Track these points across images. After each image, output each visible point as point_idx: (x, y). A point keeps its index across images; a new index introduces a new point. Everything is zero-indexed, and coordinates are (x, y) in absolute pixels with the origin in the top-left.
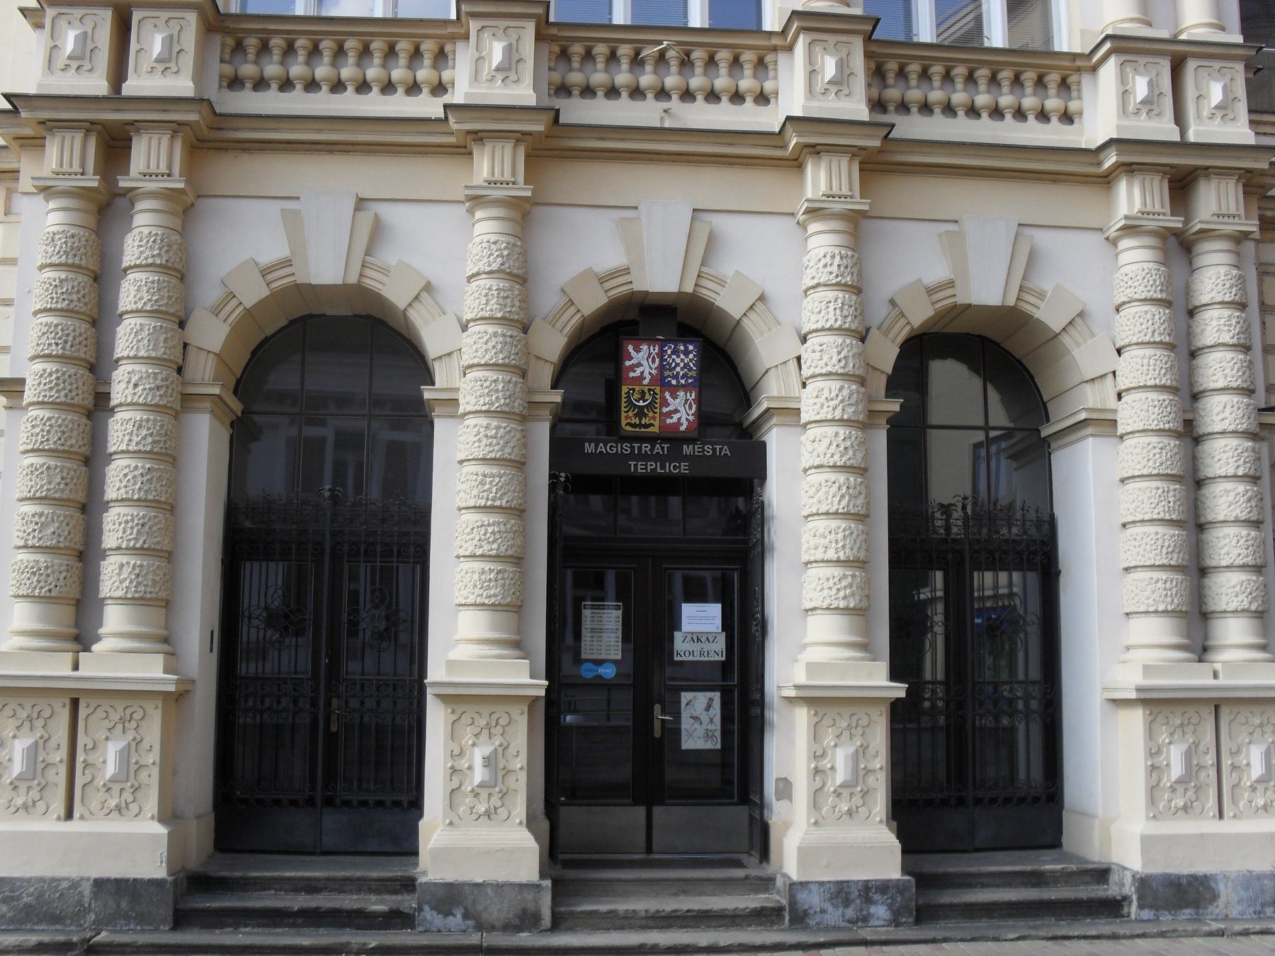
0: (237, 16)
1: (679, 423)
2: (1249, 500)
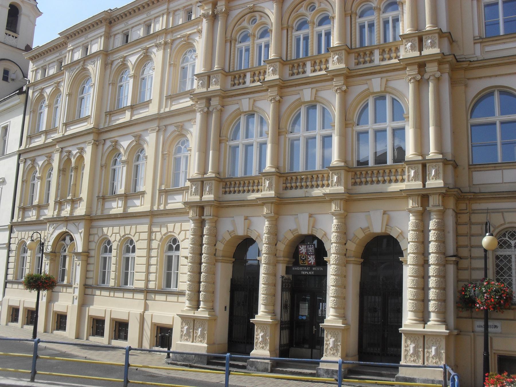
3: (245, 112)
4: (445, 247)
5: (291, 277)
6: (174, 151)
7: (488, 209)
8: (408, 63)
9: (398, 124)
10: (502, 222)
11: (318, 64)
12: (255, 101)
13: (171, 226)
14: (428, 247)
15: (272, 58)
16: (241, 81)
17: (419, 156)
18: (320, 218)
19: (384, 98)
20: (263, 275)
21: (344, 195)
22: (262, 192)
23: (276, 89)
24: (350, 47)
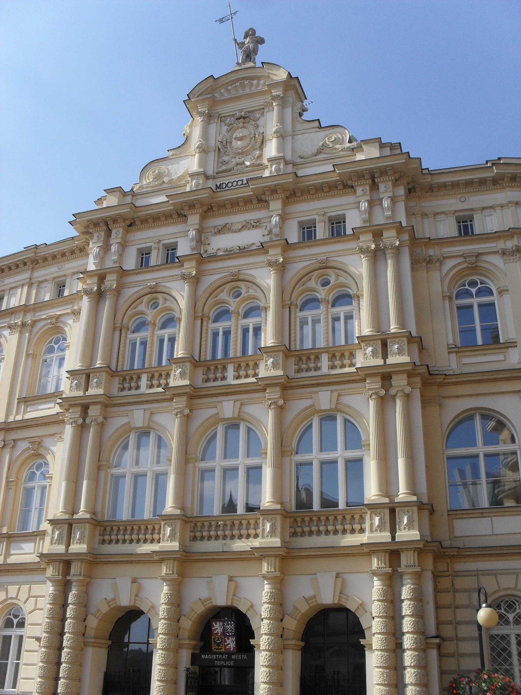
2: (416, 676)
3: (138, 428)
4: (424, 625)
5: (196, 669)
7: (477, 571)
8: (366, 374)
9: (253, 461)
10: (496, 588)
12: (152, 413)
13: (13, 590)
14: (401, 624)
15: (179, 356)
18: (244, 582)
19: (333, 418)
21: (281, 549)
23: (185, 398)
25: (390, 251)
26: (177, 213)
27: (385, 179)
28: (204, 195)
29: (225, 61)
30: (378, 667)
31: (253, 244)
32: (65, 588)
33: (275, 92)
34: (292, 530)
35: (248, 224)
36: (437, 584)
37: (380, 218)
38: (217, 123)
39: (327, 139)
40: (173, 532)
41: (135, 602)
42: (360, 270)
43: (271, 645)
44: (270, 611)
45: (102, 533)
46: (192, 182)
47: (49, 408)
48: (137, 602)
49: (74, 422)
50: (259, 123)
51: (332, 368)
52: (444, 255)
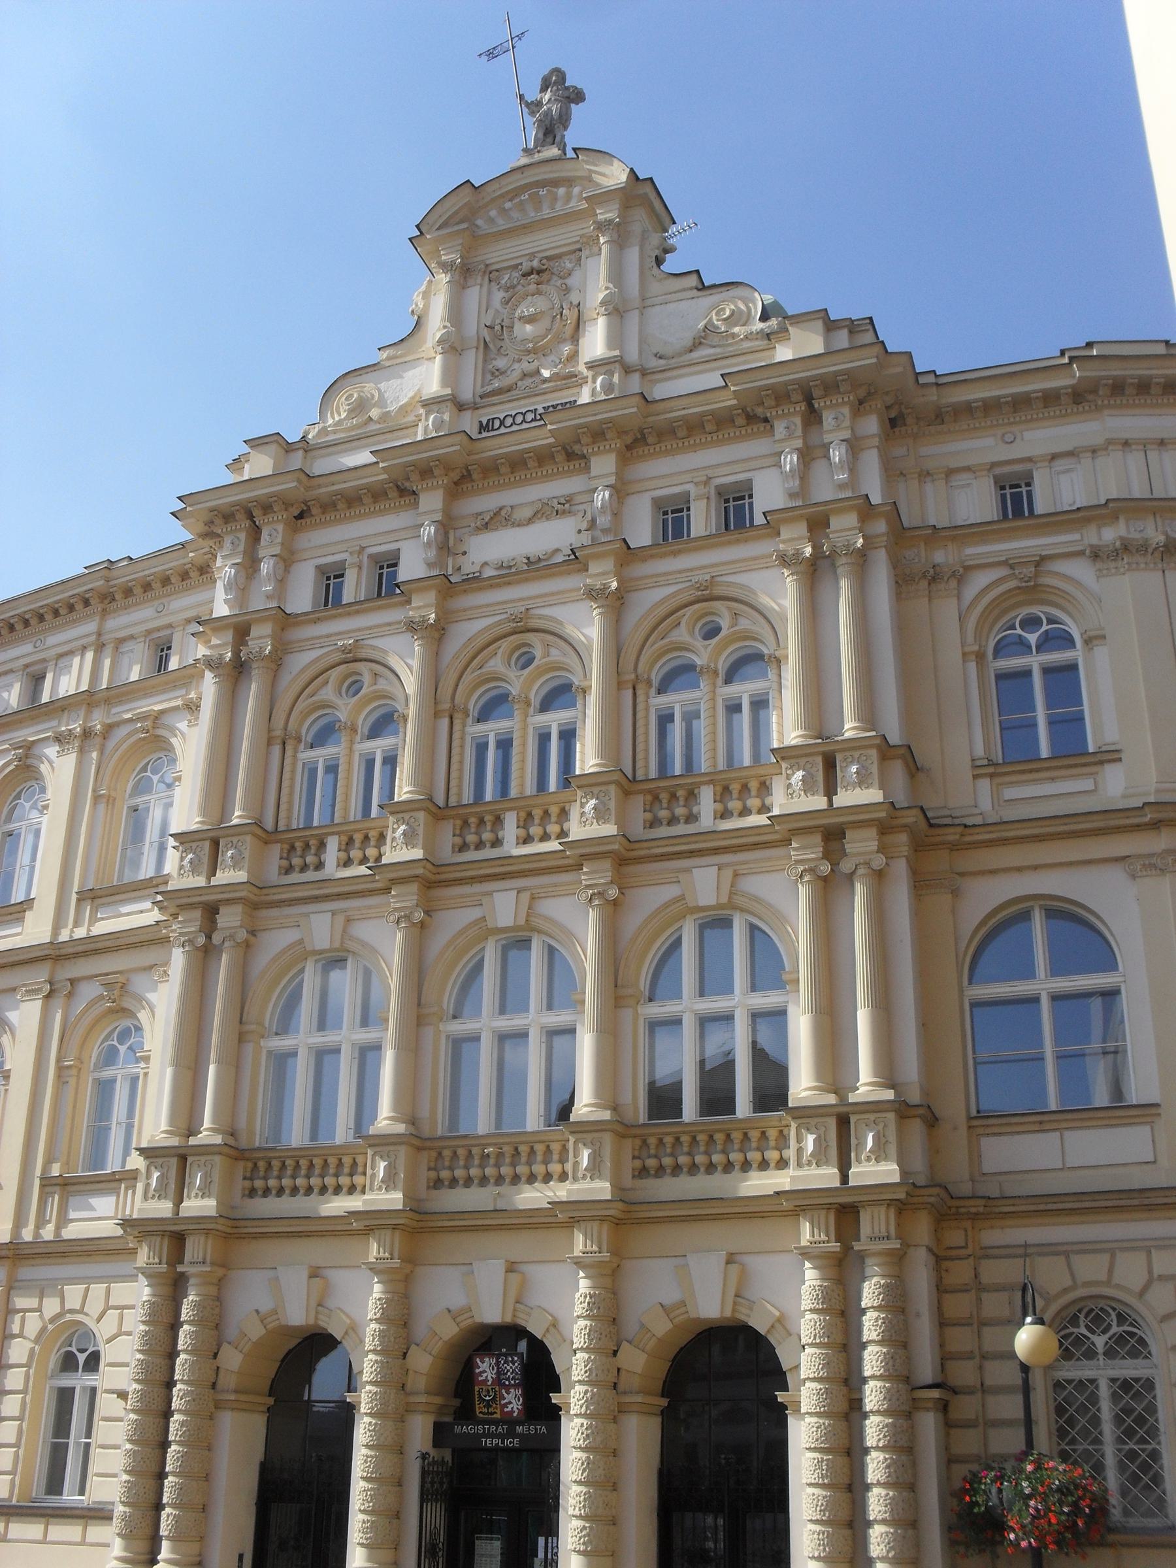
0: (298, 1154)
1: (512, 1411)
2: (888, 1467)
3: (321, 952)
4: (909, 1360)
5: (447, 1455)
6: (93, 1060)
7: (1026, 1246)
8: (794, 827)
9: (766, 1000)
10: (1068, 1282)
11: (537, 821)
12: (348, 920)
13: (73, 1294)
14: (860, 1360)
15: (404, 797)
16: (310, 859)
17: (829, 1092)
19: (725, 923)
20: (364, 1451)
22: (363, 1192)
23: (414, 888)
24: (630, 777)
25: (844, 560)
26: (398, 486)
27: (834, 402)
28: (450, 448)
29: (498, 145)
30: (809, 1449)
31: (557, 550)
32: (175, 1290)
33: (603, 214)
34: (638, 1164)
35: (546, 507)
36: (943, 1273)
37: (827, 485)
38: (481, 285)
39: (714, 313)
40: (595, 1159)
41: (316, 1318)
42: (781, 601)
43: (592, 1404)
44: (589, 1334)
45: (248, 1175)
46: (427, 419)
47: (142, 912)
48: (321, 1317)
49: (189, 941)
50: (569, 281)
51: (723, 817)
52: (967, 563)
